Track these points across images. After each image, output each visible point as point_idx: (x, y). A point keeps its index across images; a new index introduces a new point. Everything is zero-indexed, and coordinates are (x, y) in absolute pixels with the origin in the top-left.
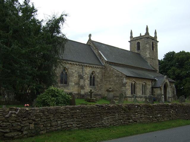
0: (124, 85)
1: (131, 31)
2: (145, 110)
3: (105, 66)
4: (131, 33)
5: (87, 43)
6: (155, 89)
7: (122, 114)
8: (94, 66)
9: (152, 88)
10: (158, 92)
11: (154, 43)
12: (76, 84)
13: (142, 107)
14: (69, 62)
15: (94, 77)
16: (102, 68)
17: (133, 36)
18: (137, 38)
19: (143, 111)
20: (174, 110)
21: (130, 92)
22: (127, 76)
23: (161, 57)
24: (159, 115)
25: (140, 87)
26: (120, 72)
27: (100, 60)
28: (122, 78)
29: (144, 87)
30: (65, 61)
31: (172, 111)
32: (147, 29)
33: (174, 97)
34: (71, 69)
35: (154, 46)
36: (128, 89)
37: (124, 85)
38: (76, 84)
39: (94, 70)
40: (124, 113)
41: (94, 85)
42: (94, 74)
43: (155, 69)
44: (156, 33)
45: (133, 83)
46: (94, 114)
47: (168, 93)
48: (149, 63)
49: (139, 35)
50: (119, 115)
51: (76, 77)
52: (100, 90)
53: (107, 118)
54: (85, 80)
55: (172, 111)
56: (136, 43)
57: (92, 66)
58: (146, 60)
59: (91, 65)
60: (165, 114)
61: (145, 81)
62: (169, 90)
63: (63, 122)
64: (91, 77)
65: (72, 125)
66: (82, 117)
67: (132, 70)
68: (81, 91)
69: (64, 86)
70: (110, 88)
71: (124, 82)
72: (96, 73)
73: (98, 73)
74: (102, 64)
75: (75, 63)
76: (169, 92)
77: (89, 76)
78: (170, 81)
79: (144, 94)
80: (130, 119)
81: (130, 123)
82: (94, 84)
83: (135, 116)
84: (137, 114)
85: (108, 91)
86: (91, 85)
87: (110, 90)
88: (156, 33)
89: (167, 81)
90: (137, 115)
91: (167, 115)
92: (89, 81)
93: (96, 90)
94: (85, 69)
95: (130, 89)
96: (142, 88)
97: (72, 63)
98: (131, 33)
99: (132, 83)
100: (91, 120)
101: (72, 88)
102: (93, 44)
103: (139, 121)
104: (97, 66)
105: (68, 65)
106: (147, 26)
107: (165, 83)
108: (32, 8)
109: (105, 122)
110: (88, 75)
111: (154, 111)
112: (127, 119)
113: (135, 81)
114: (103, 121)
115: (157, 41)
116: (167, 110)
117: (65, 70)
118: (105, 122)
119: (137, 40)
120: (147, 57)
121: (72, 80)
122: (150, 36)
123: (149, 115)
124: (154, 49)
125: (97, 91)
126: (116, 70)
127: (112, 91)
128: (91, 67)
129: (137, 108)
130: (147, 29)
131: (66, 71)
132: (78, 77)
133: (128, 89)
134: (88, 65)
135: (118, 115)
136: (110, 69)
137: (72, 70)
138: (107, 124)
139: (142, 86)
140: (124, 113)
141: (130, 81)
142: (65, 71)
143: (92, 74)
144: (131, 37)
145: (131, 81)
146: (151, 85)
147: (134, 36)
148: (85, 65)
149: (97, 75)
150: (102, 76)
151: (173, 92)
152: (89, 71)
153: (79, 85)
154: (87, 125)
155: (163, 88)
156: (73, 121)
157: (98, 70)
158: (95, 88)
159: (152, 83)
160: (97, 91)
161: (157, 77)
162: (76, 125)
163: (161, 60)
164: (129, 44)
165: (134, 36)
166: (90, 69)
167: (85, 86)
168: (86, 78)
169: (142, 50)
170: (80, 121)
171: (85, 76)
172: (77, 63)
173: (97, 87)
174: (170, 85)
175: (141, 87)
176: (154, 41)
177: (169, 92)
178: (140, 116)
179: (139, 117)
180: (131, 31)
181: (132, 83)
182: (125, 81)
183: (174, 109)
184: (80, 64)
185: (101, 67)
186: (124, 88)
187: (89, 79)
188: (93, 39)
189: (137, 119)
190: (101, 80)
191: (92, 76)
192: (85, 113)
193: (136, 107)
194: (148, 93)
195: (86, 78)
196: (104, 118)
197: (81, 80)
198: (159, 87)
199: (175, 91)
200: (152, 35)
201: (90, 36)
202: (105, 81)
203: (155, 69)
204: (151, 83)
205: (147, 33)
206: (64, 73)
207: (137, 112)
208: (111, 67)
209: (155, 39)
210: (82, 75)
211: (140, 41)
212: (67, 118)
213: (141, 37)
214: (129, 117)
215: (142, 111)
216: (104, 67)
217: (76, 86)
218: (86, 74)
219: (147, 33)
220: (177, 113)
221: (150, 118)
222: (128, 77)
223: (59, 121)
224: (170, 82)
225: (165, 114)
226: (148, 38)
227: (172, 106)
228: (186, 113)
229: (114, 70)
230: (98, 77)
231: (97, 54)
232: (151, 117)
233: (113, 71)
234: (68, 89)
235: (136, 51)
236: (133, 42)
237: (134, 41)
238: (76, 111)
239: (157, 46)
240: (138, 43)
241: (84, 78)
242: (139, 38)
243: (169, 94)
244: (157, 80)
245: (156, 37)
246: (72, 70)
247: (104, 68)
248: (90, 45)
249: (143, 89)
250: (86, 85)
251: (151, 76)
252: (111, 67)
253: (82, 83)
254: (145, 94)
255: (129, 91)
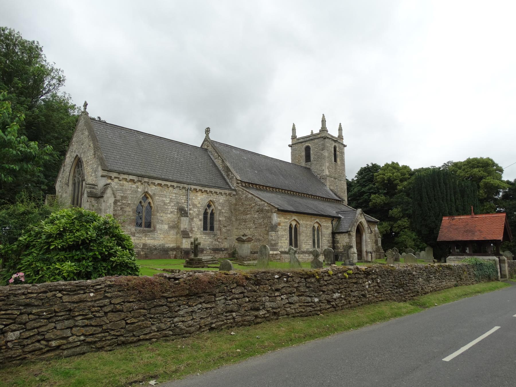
0: (274, 228)
1: (294, 125)
2: (301, 284)
3: (235, 190)
4: (294, 129)
5: (202, 145)
6: (338, 237)
7: (237, 296)
8: (212, 190)
9: (334, 234)
10: (343, 240)
11: (337, 149)
12: (172, 228)
13: (291, 277)
14: (157, 182)
15: (212, 214)
16: (230, 194)
17: (297, 135)
18: (306, 140)
19: (296, 288)
20: (373, 281)
21: (288, 242)
22: (278, 210)
23: (351, 174)
24: (336, 295)
25: (309, 232)
26: (264, 201)
27: (226, 177)
28: (269, 214)
29: (316, 232)
30: (146, 180)
31: (369, 284)
32: (324, 121)
33: (377, 250)
34: (160, 196)
35: (338, 153)
36: (283, 236)
37: (274, 228)
38: (172, 228)
39: (213, 198)
40: (240, 293)
41: (212, 229)
42: (213, 207)
43: (339, 198)
44: (340, 129)
45: (294, 223)
46: (148, 302)
47: (364, 243)
48: (328, 186)
49: (309, 134)
50: (226, 299)
51: (172, 212)
52: (225, 238)
53: (190, 309)
54: (192, 219)
55: (369, 284)
56: (303, 149)
57: (208, 189)
58: (322, 180)
59: (206, 189)
60: (351, 291)
61: (318, 220)
62: (366, 236)
63: (28, 334)
64: (206, 213)
65: (67, 338)
66: (106, 313)
67: (288, 197)
68: (182, 243)
69: (144, 232)
70: (244, 235)
71: (274, 222)
72: (216, 204)
73: (222, 205)
74: (230, 186)
75: (169, 184)
76: (366, 241)
77: (202, 212)
78: (370, 220)
79: (316, 246)
80: (258, 309)
81: (259, 320)
82: (213, 227)
83: (273, 299)
84: (277, 294)
85: (239, 240)
86: (205, 228)
87: (245, 238)
88: (340, 129)
89: (363, 220)
90: (279, 298)
91: (356, 294)
92: (200, 220)
93: (218, 239)
94: (192, 195)
95: (287, 236)
96: (311, 235)
97: (163, 183)
98: (294, 129)
99: (291, 225)
100: (134, 320)
101: (162, 236)
102: (214, 148)
103: (284, 311)
104: (218, 191)
105: (154, 187)
106: (323, 114)
107: (358, 223)
108: (361, 208)
109: (183, 322)
110: (198, 207)
111: (325, 285)
112: (251, 309)
113: (298, 220)
114: (176, 320)
115: (343, 144)
116: (355, 283)
117: (147, 198)
118: (183, 322)
119: (305, 141)
120: (324, 174)
121: (162, 219)
122: (329, 134)
123: (311, 297)
124: (338, 160)
125: (219, 242)
126: (257, 197)
127: (249, 240)
128: (206, 191)
129: (277, 279)
130: (324, 121)
131: (150, 200)
132: (176, 213)
133: (283, 236)
134: (198, 188)
135: (224, 301)
136: (246, 197)
137: (164, 199)
138: (190, 326)
139: (311, 229)
140: (240, 293)
141: (286, 220)
142: (148, 201)
143: (209, 206)
144: (294, 137)
145: (289, 219)
146: (331, 229)
147: (299, 135)
148: (193, 187)
149: (219, 208)
150: (230, 210)
151: (376, 242)
152: (202, 199)
153: (179, 229)
154: (122, 335)
155: (354, 234)
156: (71, 328)
157: (222, 199)
158: (215, 235)
159: (332, 223)
160: (219, 242)
161: (343, 212)
162: (82, 338)
163: (353, 180)
164: (290, 151)
165: (300, 134)
166: (205, 195)
167: (192, 231)
168: (195, 214)
169: (315, 161)
170: (96, 326)
171: (193, 212)
172: (175, 184)
173: (219, 232)
174: (369, 227)
175: (309, 231)
176: (337, 145)
177: (366, 241)
178: (288, 299)
179: (284, 302)
180: (294, 125)
181: (291, 225)
182: (276, 218)
183: (372, 279)
184: (182, 185)
185: (227, 192)
186: (273, 233)
187: (201, 217)
188: (212, 137)
189: (279, 307)
190: (229, 219)
191: (209, 211)
192: (118, 301)
193: (276, 276)
194: (325, 243)
195: (195, 214)
196: (180, 310)
197: (182, 218)
198: (347, 232)
199: (380, 240)
200: (333, 132)
201: (208, 131)
202: (236, 220)
203: (339, 198)
204: (331, 225)
205: (324, 129)
206: (145, 204)
207: (277, 290)
208: (249, 193)
209: (339, 141)
210: (186, 209)
211: (310, 145)
212: (48, 319)
213: (312, 138)
214: (257, 305)
215: (293, 287)
216: (234, 193)
217: (173, 232)
218: (194, 206)
219: (324, 129)
220: (379, 287)
221: (314, 303)
222: (282, 211)
223: (13, 331)
224: (369, 222)
225: (351, 291)
226: (325, 138)
227: (368, 272)
228: (402, 287)
229: (254, 197)
230: (221, 213)
231: (221, 167)
232: (316, 300)
233: (251, 199)
234: (154, 239)
235: (303, 164)
236: (296, 147)
237: (300, 145)
238: (84, 296)
239: (342, 153)
240: (308, 149)
241: (190, 214)
242: (308, 139)
243: (366, 245)
244: (343, 217)
245: (341, 137)
246: (164, 199)
247: (234, 195)
248: (206, 150)
249: (314, 235)
250: (195, 229)
251: (331, 210)
252: (249, 193)
253: (184, 224)
254: (318, 247)
255: (285, 241)
